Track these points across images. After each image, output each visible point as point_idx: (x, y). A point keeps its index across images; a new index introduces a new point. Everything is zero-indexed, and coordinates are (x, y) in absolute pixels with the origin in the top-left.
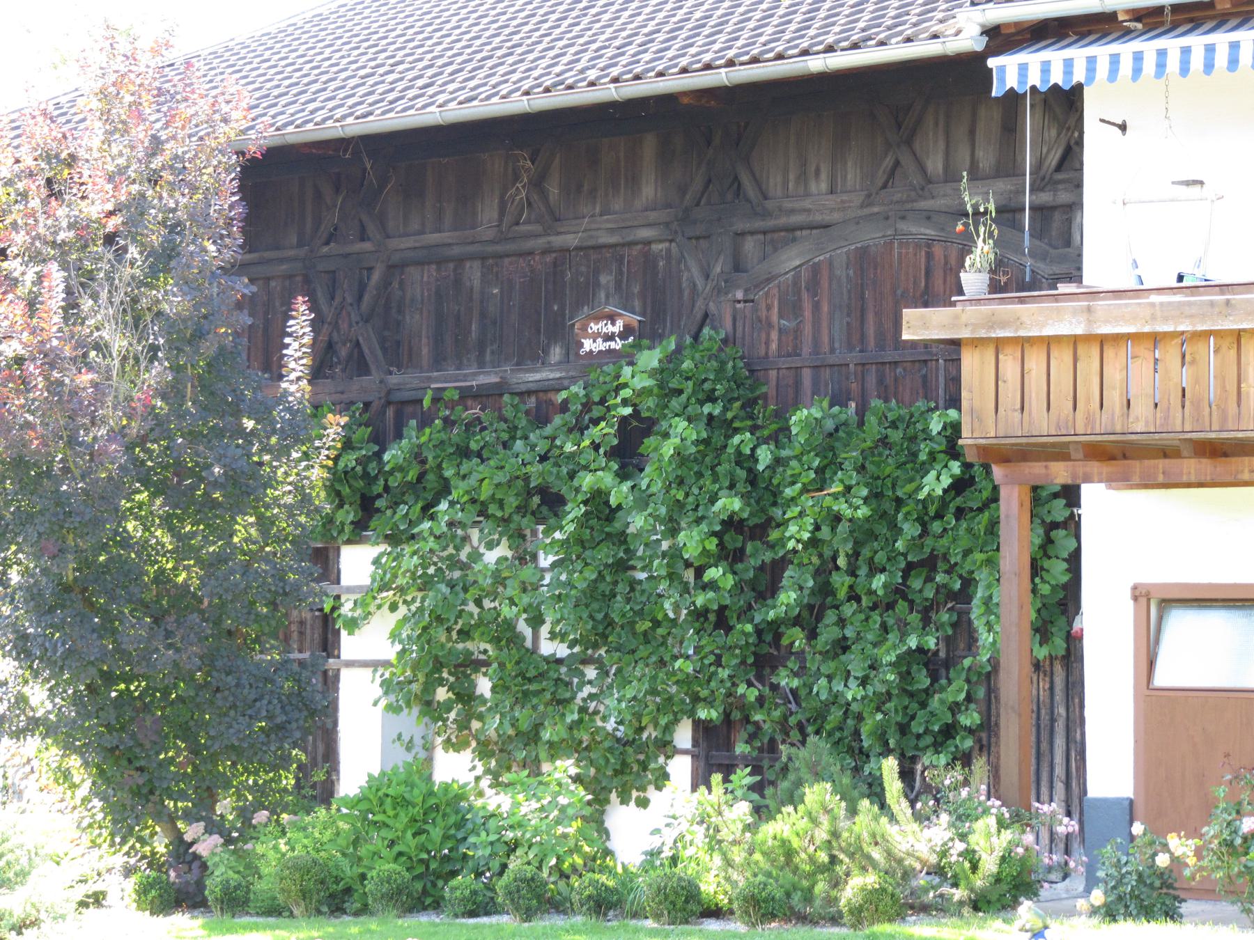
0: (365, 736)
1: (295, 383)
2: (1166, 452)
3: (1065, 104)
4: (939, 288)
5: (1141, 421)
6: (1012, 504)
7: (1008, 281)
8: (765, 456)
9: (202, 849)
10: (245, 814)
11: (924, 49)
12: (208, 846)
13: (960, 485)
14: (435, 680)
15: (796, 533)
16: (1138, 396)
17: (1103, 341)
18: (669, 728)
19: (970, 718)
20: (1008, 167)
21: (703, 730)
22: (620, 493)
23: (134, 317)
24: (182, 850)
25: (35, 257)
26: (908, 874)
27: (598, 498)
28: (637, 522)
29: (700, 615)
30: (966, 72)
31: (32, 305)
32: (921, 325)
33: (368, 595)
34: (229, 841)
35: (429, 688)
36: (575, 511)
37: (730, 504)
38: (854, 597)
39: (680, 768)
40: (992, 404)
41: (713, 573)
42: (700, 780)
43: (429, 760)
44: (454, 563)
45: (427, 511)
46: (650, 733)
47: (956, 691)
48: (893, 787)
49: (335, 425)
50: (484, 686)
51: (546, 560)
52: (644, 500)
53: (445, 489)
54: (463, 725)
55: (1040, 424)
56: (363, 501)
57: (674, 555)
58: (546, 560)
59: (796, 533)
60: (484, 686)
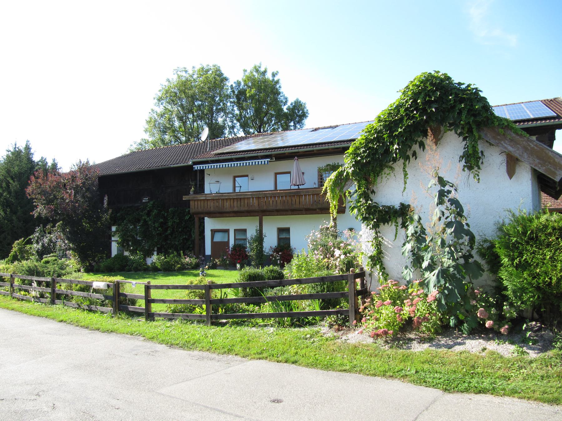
0: (115, 249)
1: (105, 205)
2: (215, 213)
3: (202, 172)
4: (188, 193)
5: (212, 209)
6: (196, 219)
7: (195, 192)
8: (166, 214)
9: (93, 264)
10: (99, 260)
11: (185, 164)
12: (94, 264)
13: (190, 218)
14: (123, 245)
15: (170, 224)
16: (211, 206)
17: (207, 200)
18: (154, 248)
19: (191, 246)
20: (196, 179)
21: (158, 248)
22: (148, 219)
23: (83, 197)
24: (90, 264)
25: (70, 189)
26: (184, 265)
27: (145, 220)
28: (150, 223)
29: (157, 234)
30: (191, 167)
31: (70, 195)
32: (185, 198)
33: (115, 232)
34: (97, 263)
35: (123, 243)
36: (142, 222)
37: (161, 220)
38: (177, 231)
39: (155, 253)
40: (194, 207)
41: (159, 229)
42: (158, 254)
43: (123, 253)
44: (126, 228)
45: (123, 222)
46: (152, 249)
47: (190, 243)
48: (182, 254)
49: (110, 211)
50: (130, 243)
51: (138, 228)
52: (150, 220)
53: (125, 219)
54: (127, 248)
55: (200, 210)
56: (114, 220)
57: (154, 226)
58: (138, 228)
59: (170, 224)
60: (130, 243)
